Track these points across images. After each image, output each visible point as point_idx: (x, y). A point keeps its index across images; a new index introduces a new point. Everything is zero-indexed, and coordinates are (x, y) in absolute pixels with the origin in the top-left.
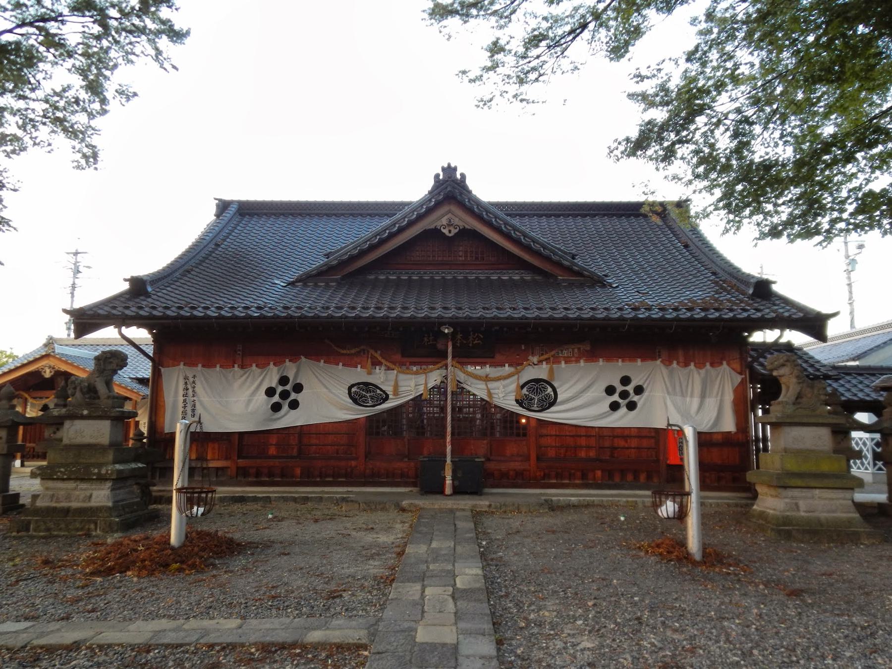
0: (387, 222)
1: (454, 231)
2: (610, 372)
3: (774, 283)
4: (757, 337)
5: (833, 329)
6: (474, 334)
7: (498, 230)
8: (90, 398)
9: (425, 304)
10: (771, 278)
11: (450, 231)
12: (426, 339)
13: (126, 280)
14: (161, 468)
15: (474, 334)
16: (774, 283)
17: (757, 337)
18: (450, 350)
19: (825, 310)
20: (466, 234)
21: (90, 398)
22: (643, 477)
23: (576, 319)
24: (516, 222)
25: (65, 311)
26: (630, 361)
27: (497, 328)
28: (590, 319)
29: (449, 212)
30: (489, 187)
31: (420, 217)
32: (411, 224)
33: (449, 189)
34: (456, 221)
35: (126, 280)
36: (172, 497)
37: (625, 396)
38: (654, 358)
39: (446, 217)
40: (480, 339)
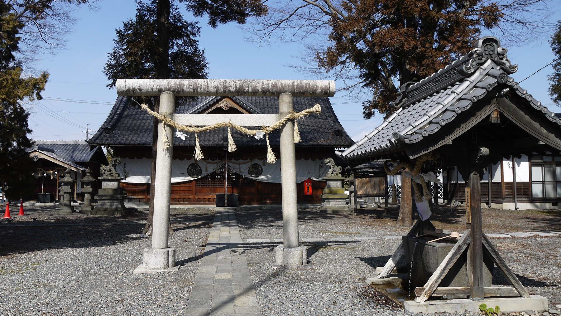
1: (227, 109)
29: (225, 101)
34: (228, 105)
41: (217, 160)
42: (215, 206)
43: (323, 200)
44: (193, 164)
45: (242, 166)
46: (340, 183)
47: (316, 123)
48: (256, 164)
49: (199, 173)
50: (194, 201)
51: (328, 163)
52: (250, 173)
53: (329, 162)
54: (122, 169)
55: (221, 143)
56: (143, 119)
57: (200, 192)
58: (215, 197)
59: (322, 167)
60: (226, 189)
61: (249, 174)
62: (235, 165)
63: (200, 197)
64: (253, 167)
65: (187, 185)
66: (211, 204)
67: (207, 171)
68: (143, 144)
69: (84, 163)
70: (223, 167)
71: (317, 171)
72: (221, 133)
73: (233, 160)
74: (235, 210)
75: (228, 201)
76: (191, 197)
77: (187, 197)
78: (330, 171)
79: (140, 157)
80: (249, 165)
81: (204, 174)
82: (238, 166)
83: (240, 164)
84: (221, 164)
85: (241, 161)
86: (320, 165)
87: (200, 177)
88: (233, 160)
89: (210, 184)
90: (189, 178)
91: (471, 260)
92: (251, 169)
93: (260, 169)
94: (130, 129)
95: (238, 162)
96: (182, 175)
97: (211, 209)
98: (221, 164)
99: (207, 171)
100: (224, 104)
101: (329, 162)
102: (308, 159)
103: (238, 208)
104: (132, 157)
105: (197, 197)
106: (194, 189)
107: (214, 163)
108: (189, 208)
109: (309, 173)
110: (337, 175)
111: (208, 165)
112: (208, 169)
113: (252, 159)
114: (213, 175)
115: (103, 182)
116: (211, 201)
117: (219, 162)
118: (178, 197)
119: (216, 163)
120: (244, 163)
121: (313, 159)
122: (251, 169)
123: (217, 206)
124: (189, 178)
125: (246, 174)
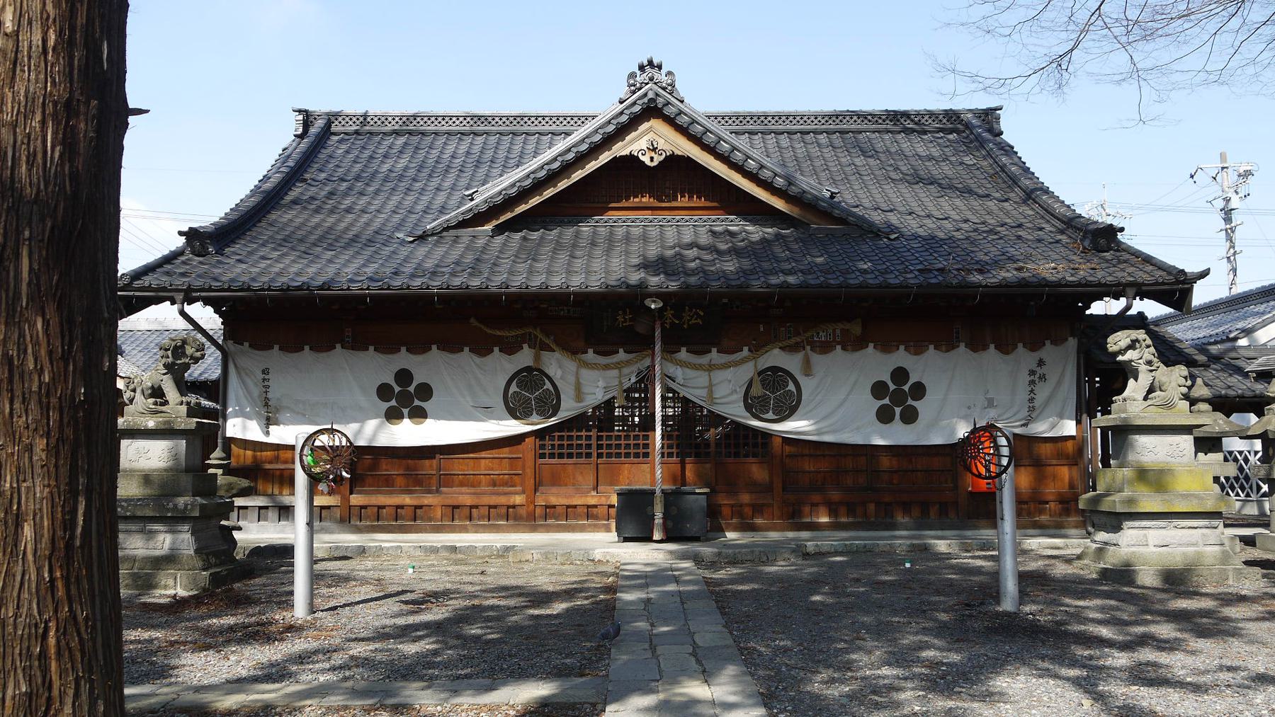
0: (561, 145)
1: (658, 159)
2: (876, 364)
3: (1122, 230)
4: (1097, 308)
5: (1201, 294)
6: (690, 310)
7: (724, 159)
8: (155, 404)
9: (597, 265)
10: (1117, 223)
11: (652, 159)
12: (620, 318)
13: (181, 233)
14: (240, 508)
15: (690, 310)
16: (1122, 230)
17: (1097, 308)
18: (658, 333)
19: (1191, 268)
20: (675, 163)
21: (155, 404)
22: (933, 512)
23: (840, 286)
24: (742, 142)
25: (1204, 274)
26: (316, 348)
27: (725, 301)
28: (860, 286)
29: (650, 130)
30: (703, 96)
31: (609, 140)
32: (595, 150)
33: (651, 95)
34: (661, 144)
35: (181, 233)
36: (663, 438)
37: (898, 399)
38: (951, 347)
39: (646, 138)
40: (699, 316)
41: (622, 355)
42: (613, 536)
43: (1115, 521)
44: (528, 369)
45: (719, 376)
46: (1186, 442)
47: (1007, 214)
48: (775, 369)
49: (550, 404)
50: (532, 517)
51: (1123, 351)
52: (754, 405)
53: (1132, 346)
54: (256, 392)
55: (635, 278)
56: (348, 210)
57: (556, 481)
58: (614, 500)
59: (1043, 378)
60: (653, 474)
61: (748, 408)
62: (691, 373)
63: (554, 500)
64: (764, 384)
65: (505, 452)
66: (595, 528)
67: (579, 396)
68: (321, 288)
69: (205, 383)
70: (645, 382)
71: (1023, 395)
72: (634, 247)
73: (683, 354)
74: (697, 559)
75: (665, 518)
76: (518, 500)
77: (502, 500)
78: (1134, 389)
79: (323, 345)
80: (746, 372)
81: (569, 408)
82: (701, 378)
83: (711, 368)
84: (635, 368)
85: (714, 356)
86: (1032, 373)
87: (553, 421)
88: (683, 354)
89: (594, 451)
90: (513, 427)
91: (20, 294)
92: (757, 390)
93: (791, 387)
94: (287, 242)
95: (704, 360)
96: (485, 412)
97: (598, 554)
98: (635, 368)
99: (579, 396)
100: (643, 144)
101: (1132, 346)
102: (985, 348)
103: (706, 550)
104: (292, 346)
105: (540, 501)
106: (530, 472)
107: (607, 367)
108: (507, 549)
109: (990, 403)
110: (1168, 405)
111: (586, 374)
112: (586, 389)
113: (758, 348)
114: (603, 417)
115: (124, 443)
116: (596, 517)
117: (628, 363)
118: (467, 500)
119: (618, 366)
120: (726, 366)
121: (1005, 348)
122: (757, 390)
123: (654, 430)
124: (513, 427)
125: (735, 410)
